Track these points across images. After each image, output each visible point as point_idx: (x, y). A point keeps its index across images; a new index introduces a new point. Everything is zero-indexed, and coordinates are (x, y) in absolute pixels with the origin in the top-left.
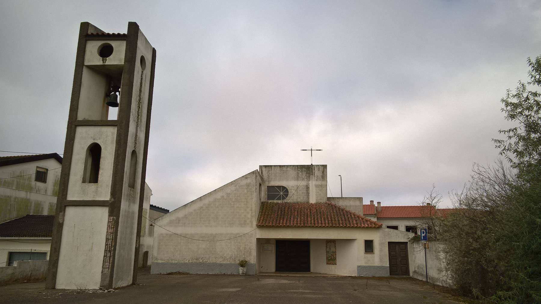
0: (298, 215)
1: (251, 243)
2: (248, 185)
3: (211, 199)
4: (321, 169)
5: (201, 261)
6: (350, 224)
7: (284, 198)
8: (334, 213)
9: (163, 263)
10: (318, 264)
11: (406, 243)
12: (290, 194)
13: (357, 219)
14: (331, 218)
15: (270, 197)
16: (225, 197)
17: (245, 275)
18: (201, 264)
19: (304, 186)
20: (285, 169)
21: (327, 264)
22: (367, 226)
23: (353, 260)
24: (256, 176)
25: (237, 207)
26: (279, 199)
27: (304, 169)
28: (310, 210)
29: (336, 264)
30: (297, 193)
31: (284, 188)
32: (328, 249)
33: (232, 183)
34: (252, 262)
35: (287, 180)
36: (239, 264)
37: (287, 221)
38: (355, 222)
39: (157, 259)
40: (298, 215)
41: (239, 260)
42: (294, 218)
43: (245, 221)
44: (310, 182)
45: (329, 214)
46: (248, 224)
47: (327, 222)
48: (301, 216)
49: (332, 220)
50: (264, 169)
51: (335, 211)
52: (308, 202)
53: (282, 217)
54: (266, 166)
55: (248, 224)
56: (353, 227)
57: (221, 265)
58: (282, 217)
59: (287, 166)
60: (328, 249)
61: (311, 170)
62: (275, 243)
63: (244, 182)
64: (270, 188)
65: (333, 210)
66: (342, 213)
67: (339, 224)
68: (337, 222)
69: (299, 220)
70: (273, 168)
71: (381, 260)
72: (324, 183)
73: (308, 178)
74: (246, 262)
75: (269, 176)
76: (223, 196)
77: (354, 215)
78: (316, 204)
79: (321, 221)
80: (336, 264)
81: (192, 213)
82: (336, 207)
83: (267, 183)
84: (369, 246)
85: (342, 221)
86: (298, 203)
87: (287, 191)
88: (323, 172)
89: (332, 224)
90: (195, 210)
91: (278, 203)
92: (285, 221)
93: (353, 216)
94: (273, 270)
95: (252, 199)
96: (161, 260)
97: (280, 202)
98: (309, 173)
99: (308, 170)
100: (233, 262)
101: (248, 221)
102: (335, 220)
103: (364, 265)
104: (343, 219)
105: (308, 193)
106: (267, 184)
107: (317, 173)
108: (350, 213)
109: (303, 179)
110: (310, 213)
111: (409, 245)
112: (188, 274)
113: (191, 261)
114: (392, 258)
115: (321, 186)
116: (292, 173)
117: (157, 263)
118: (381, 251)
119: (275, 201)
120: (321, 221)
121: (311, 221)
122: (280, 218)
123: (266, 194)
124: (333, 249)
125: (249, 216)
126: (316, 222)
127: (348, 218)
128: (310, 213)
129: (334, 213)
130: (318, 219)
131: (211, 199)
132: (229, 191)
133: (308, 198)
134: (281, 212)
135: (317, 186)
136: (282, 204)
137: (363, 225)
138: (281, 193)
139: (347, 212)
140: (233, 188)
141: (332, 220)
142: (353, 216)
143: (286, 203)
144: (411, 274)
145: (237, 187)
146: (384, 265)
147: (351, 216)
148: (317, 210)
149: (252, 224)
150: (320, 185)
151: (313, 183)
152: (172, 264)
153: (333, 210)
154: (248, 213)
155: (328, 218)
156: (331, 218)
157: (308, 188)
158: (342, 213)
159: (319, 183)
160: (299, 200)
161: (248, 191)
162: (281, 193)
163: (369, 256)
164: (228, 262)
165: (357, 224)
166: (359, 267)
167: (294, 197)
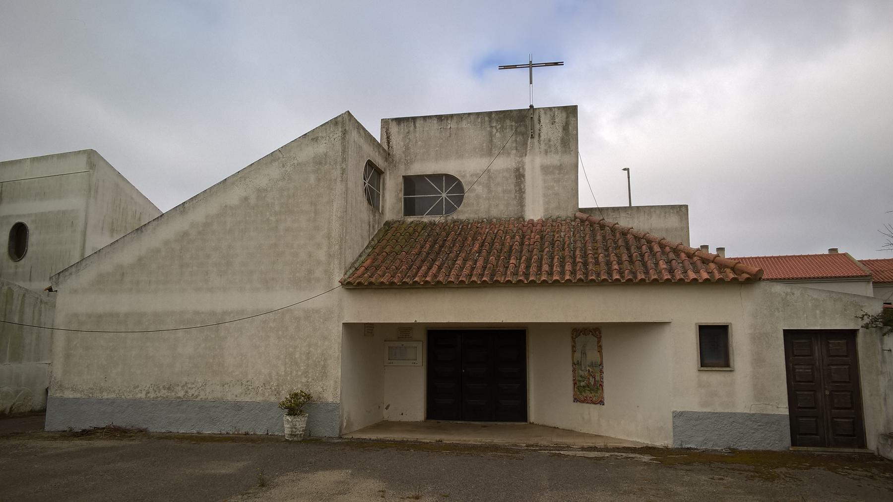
0: (480, 252)
1: (325, 338)
2: (319, 161)
3: (213, 207)
4: (560, 118)
5: (181, 394)
6: (647, 273)
7: (451, 209)
8: (595, 241)
9: (76, 400)
10: (550, 400)
11: (853, 333)
12: (469, 196)
13: (672, 256)
14: (585, 256)
15: (410, 208)
16: (253, 201)
17: (309, 439)
18: (180, 403)
19: (507, 170)
20: (452, 124)
21: (576, 400)
22: (705, 276)
23: (659, 393)
24: (345, 133)
25: (287, 230)
26: (437, 211)
27: (508, 122)
28: (523, 237)
29: (602, 403)
30: (490, 191)
31: (450, 178)
32: (578, 355)
33: (272, 157)
34: (330, 400)
35: (460, 156)
36: (282, 405)
37: (440, 268)
38: (663, 265)
39: (61, 387)
40: (480, 252)
41: (307, 385)
42: (465, 260)
43: (310, 272)
44: (527, 159)
45: (579, 244)
46: (318, 280)
47: (568, 267)
48: (489, 253)
49: (585, 264)
50: (394, 129)
51: (599, 237)
52: (520, 218)
53: (432, 256)
54: (399, 121)
55: (318, 280)
56: (656, 283)
57: (238, 407)
58: (432, 256)
59: (461, 117)
60: (578, 355)
61: (528, 122)
62: (423, 336)
63: (309, 152)
64: (410, 183)
65: (594, 235)
66: (620, 242)
67: (610, 274)
68: (603, 267)
69: (480, 263)
70: (419, 123)
71: (759, 392)
72: (567, 159)
73: (522, 148)
74: (308, 397)
75: (407, 148)
76: (246, 199)
77: (662, 246)
78: (543, 223)
79: (551, 266)
80: (602, 403)
81: (158, 251)
82: (602, 227)
83: (402, 167)
84: (714, 344)
85: (620, 263)
86: (490, 222)
87: (459, 187)
88: (566, 128)
89: (586, 274)
90: (167, 243)
91: (432, 224)
92: (434, 269)
93: (657, 248)
94: (416, 409)
95: (330, 202)
96: (74, 389)
97: (437, 219)
98: (523, 134)
99: (521, 123)
100: (273, 399)
101: (318, 273)
102: (597, 263)
103: (696, 408)
104: (625, 257)
105: (520, 191)
106: (403, 171)
107: (548, 131)
108: (649, 242)
109: (504, 151)
110: (522, 244)
111: (861, 340)
112: (143, 432)
113: (152, 395)
114: (798, 385)
115: (560, 168)
116: (474, 135)
117: (61, 398)
118: (758, 360)
119: (426, 219)
120: (551, 266)
121: (517, 267)
122: (423, 261)
123: (399, 200)
124: (592, 356)
125: (322, 255)
126: (533, 269)
127: (642, 255)
128: (522, 244)
129: (595, 241)
130: (540, 260)
131: (213, 207)
132: (262, 181)
133: (521, 204)
134: (432, 247)
135: (546, 170)
136: (443, 226)
137: (692, 275)
138: (444, 195)
139: (637, 238)
140: (274, 172)
141: (585, 264)
142: (657, 248)
143: (454, 222)
144: (873, 443)
145: (288, 168)
146: (770, 410)
147: (651, 249)
148: (542, 238)
149: (330, 280)
150: (555, 167)
151: (534, 163)
152: (100, 401)
153: (594, 235)
154: (319, 246)
155: (574, 257)
156: (585, 256)
157: (519, 175)
158: (620, 242)
159: (554, 159)
160: (495, 213)
161: (319, 180)
162: (444, 195)
163: (715, 378)
164: (259, 399)
165: (671, 271)
166: (677, 415)
167: (477, 206)
